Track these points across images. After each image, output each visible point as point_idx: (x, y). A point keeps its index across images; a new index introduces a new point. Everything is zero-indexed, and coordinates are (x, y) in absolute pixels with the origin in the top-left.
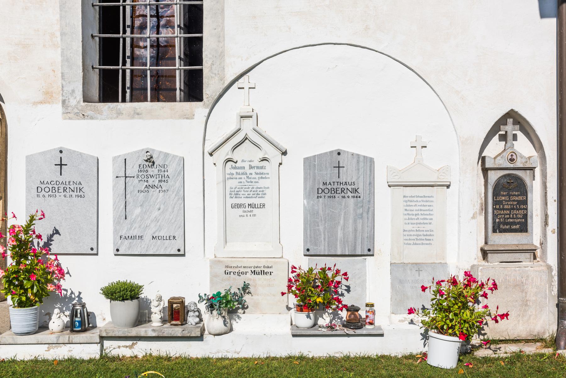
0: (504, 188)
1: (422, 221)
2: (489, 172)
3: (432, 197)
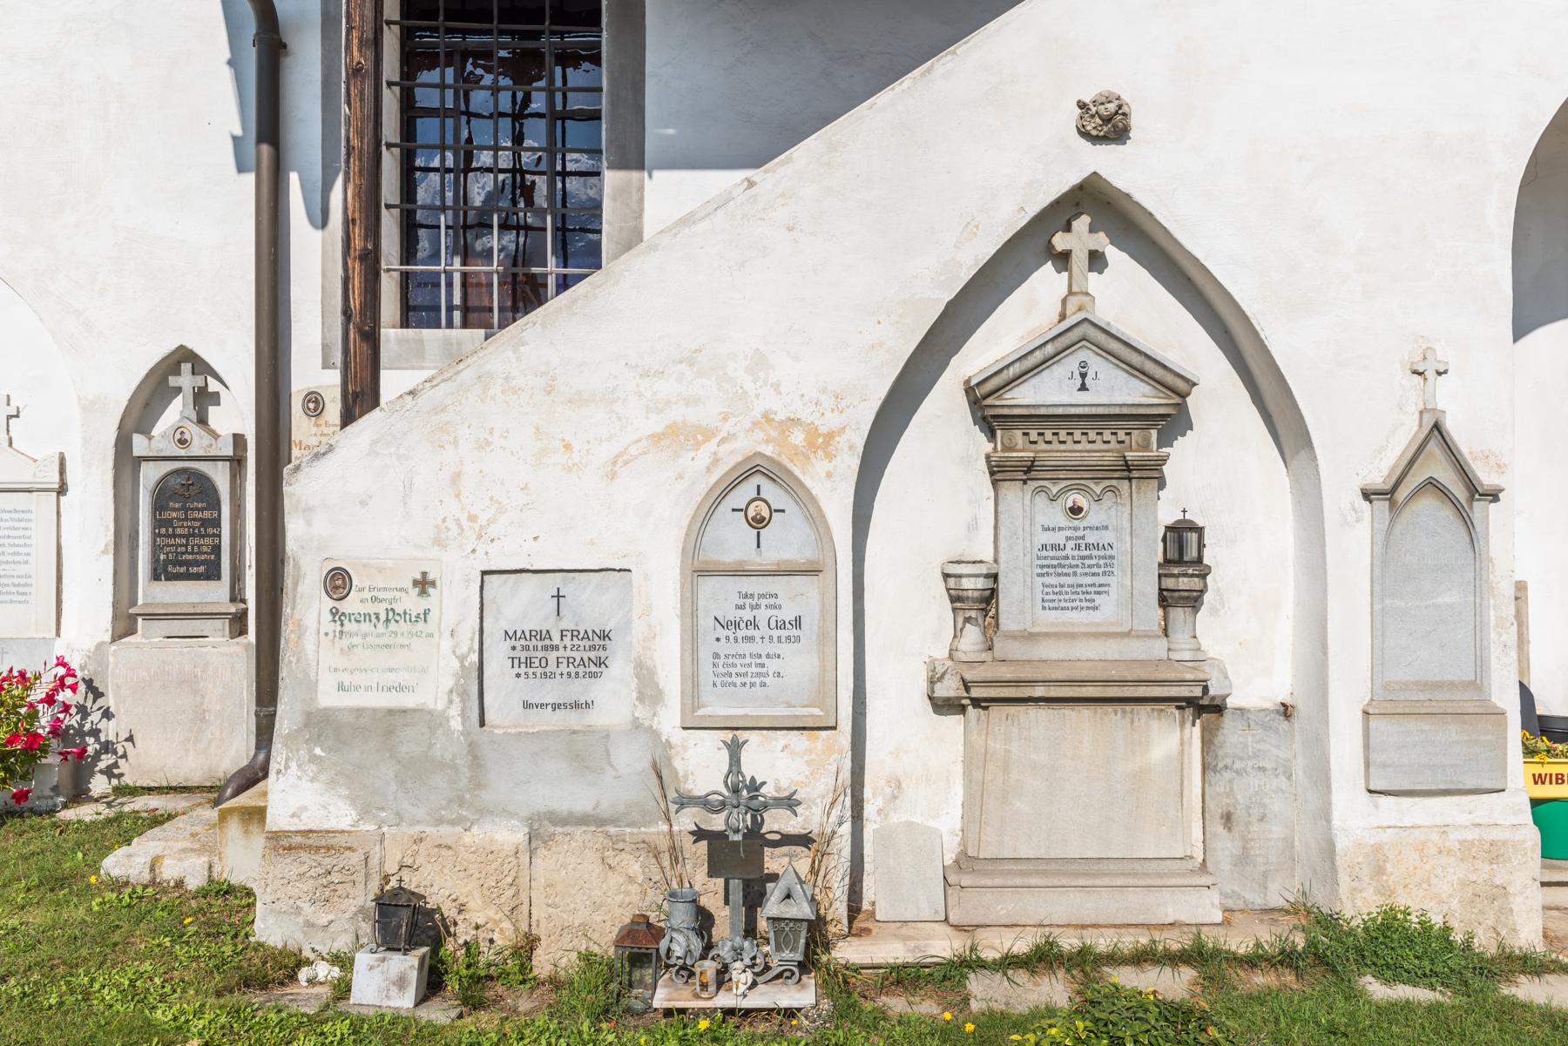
0: (174, 496)
1: (10, 558)
2: (144, 464)
3: (29, 511)
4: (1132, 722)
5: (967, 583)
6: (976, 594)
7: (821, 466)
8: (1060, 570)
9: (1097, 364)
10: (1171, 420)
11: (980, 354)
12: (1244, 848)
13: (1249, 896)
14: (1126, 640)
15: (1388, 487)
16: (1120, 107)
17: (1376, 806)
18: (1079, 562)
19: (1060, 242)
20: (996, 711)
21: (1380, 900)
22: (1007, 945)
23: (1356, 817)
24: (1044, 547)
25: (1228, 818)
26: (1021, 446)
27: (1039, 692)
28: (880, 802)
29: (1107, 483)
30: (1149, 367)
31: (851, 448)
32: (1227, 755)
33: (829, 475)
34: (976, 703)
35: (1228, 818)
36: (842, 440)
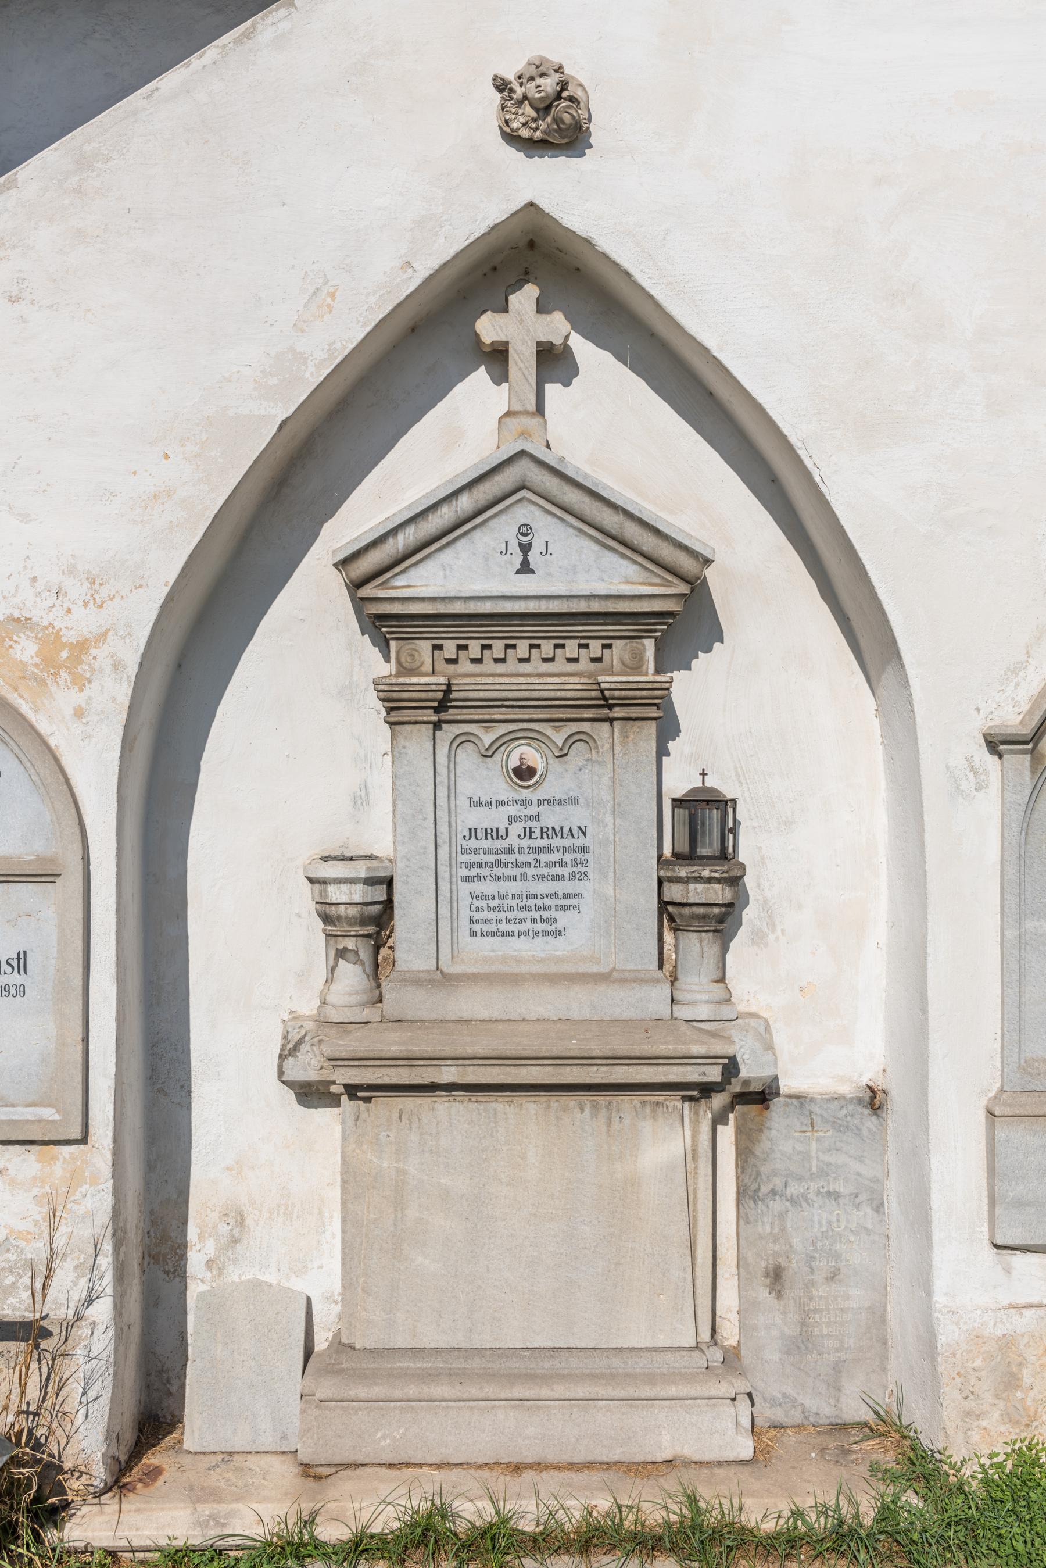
4: (609, 1123)
5: (337, 894)
6: (353, 911)
7: (65, 698)
8: (499, 871)
9: (548, 530)
10: (685, 621)
11: (366, 511)
12: (803, 1324)
13: (810, 1403)
14: (602, 988)
15: (1027, 730)
16: (564, 85)
17: (1008, 1270)
18: (530, 858)
19: (489, 328)
20: (382, 1103)
21: (1011, 1432)
22: (365, 1516)
23: (970, 1288)
24: (473, 833)
25: (776, 1276)
26: (428, 666)
27: (448, 1074)
28: (210, 1248)
29: (574, 727)
30: (632, 532)
31: (117, 666)
32: (775, 1173)
33: (79, 713)
34: (352, 1091)
35: (776, 1276)
36: (100, 654)
